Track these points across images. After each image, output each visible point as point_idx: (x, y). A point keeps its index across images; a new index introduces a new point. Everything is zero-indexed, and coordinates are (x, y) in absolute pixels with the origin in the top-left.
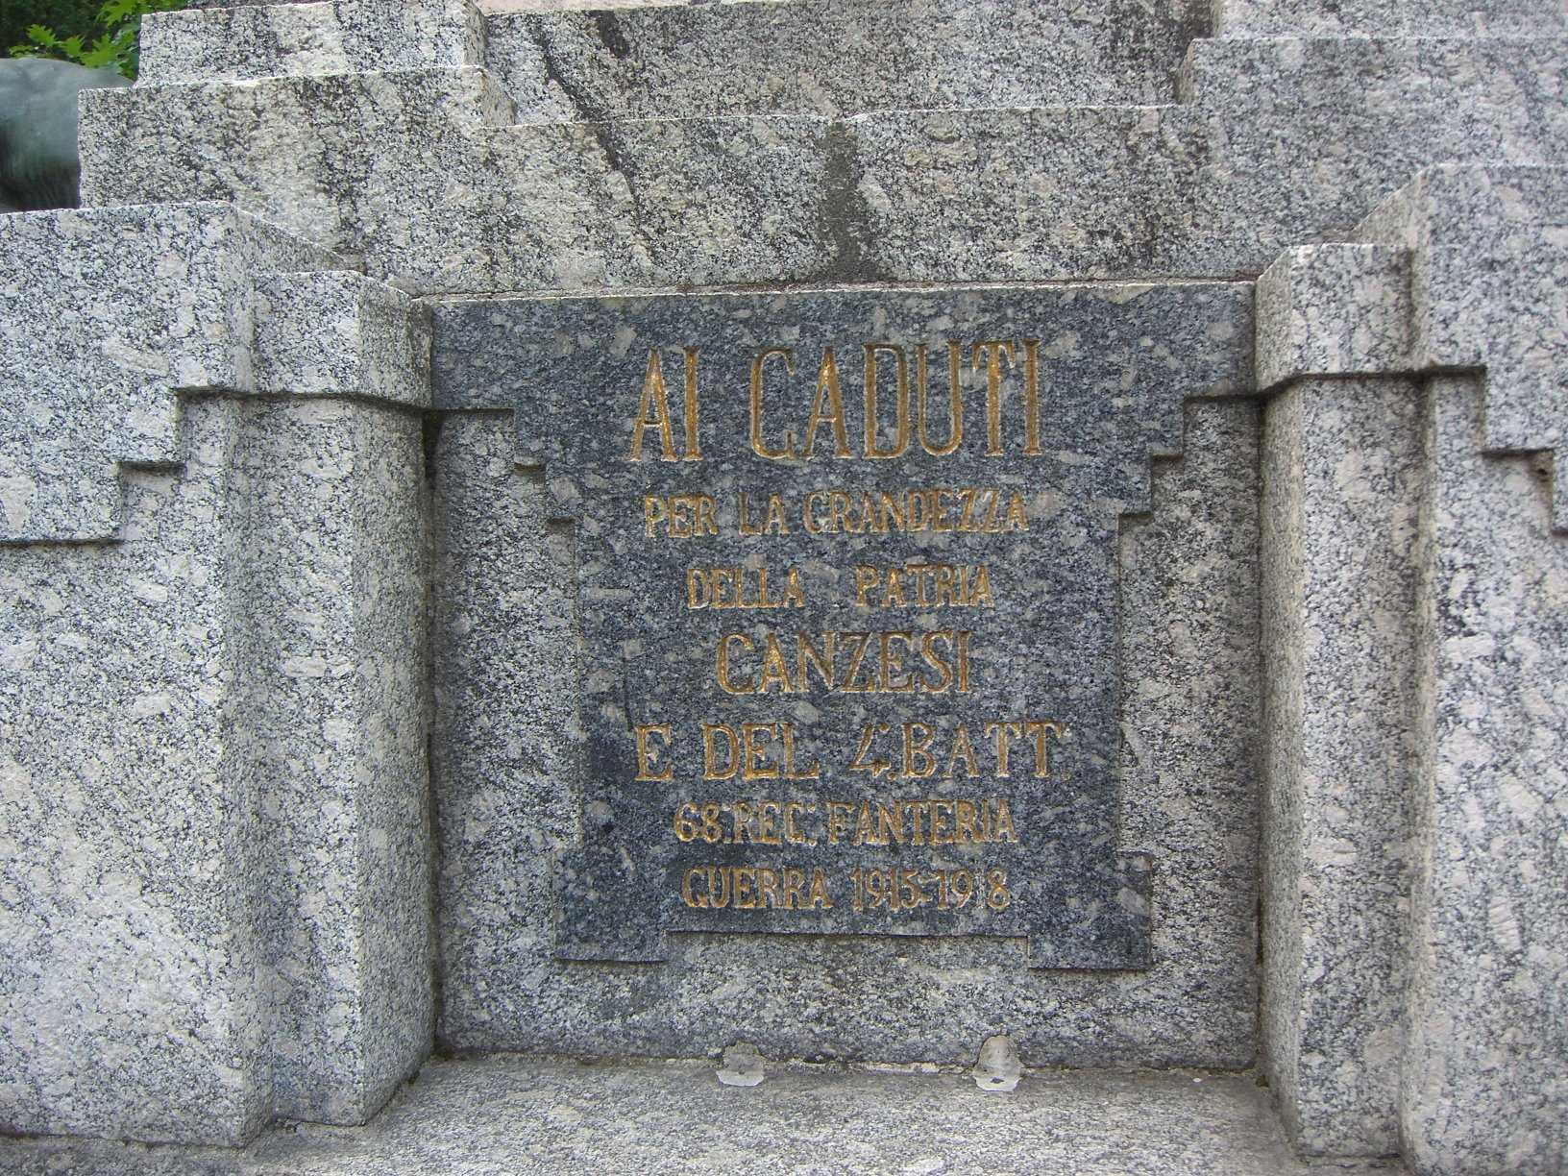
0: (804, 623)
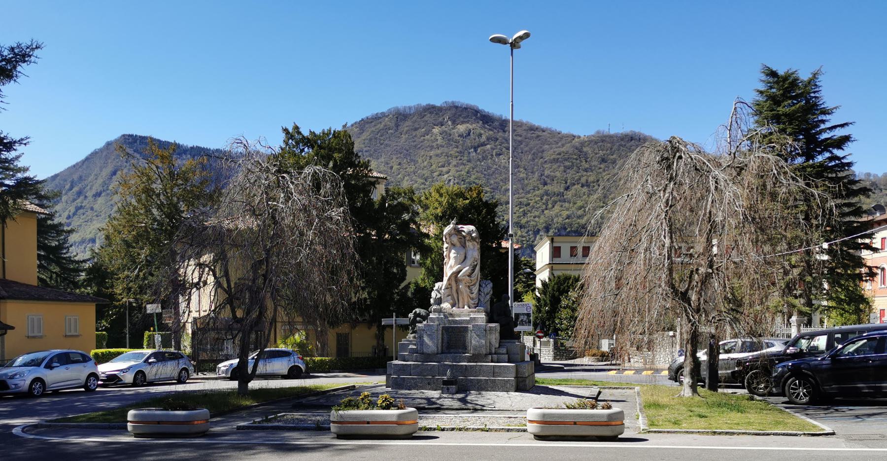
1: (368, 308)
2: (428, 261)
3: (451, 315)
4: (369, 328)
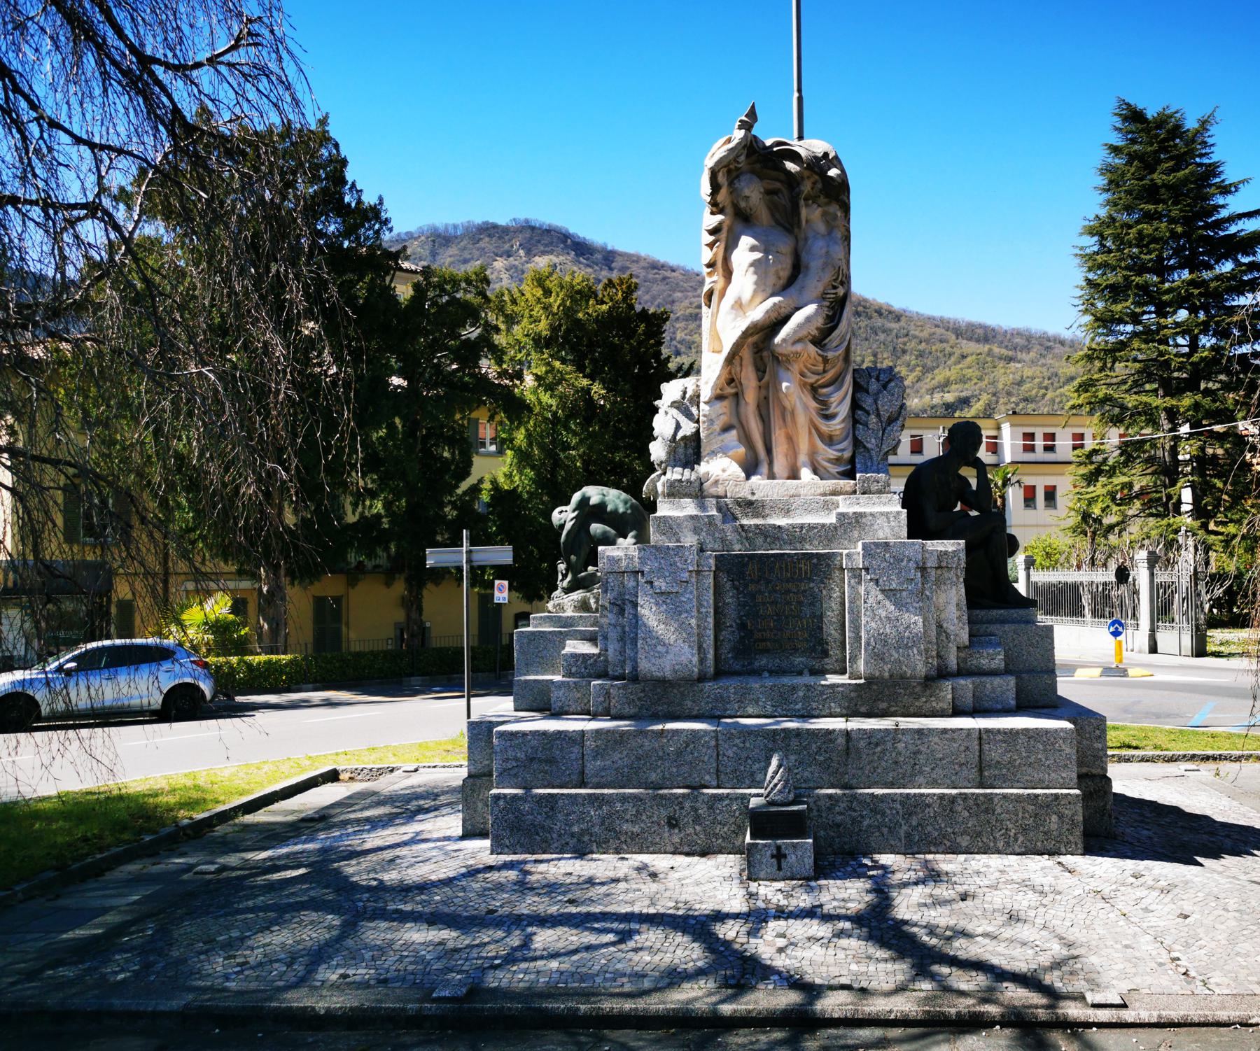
0: (774, 603)
1: (383, 539)
2: (520, 436)
3: (749, 505)
4: (388, 584)
